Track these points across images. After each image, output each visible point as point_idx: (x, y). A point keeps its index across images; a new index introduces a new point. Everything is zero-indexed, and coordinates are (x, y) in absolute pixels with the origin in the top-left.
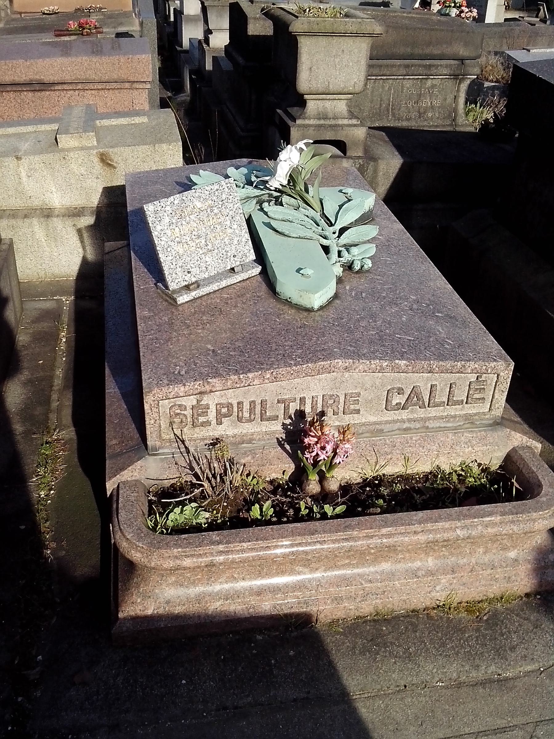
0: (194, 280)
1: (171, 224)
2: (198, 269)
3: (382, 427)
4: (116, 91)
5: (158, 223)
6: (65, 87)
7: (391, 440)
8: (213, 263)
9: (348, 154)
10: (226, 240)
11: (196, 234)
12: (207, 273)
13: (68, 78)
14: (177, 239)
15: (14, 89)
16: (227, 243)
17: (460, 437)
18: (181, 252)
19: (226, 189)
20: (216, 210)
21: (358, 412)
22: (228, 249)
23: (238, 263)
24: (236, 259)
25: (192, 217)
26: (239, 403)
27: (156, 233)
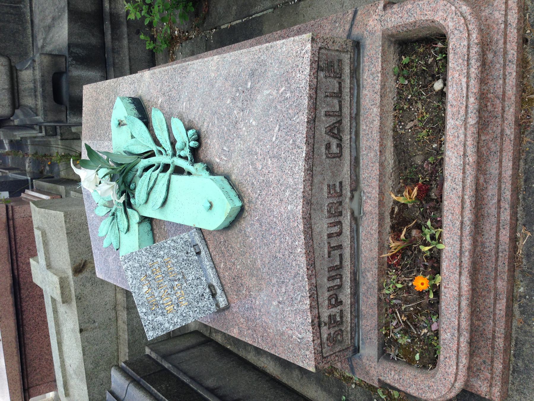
0: (208, 290)
1: (163, 314)
2: (199, 286)
3: (353, 158)
4: (16, 230)
5: (162, 327)
6: (15, 267)
7: (364, 149)
8: (193, 273)
9: (64, 70)
10: (174, 262)
11: (170, 290)
12: (202, 278)
13: (8, 267)
14: (175, 308)
15: (19, 303)
16: (176, 260)
17: (368, 83)
18: (185, 303)
19: (130, 263)
20: (149, 272)
21: (341, 183)
22: (181, 259)
23: (192, 249)
24: (189, 251)
26: (328, 291)
27: (171, 327)
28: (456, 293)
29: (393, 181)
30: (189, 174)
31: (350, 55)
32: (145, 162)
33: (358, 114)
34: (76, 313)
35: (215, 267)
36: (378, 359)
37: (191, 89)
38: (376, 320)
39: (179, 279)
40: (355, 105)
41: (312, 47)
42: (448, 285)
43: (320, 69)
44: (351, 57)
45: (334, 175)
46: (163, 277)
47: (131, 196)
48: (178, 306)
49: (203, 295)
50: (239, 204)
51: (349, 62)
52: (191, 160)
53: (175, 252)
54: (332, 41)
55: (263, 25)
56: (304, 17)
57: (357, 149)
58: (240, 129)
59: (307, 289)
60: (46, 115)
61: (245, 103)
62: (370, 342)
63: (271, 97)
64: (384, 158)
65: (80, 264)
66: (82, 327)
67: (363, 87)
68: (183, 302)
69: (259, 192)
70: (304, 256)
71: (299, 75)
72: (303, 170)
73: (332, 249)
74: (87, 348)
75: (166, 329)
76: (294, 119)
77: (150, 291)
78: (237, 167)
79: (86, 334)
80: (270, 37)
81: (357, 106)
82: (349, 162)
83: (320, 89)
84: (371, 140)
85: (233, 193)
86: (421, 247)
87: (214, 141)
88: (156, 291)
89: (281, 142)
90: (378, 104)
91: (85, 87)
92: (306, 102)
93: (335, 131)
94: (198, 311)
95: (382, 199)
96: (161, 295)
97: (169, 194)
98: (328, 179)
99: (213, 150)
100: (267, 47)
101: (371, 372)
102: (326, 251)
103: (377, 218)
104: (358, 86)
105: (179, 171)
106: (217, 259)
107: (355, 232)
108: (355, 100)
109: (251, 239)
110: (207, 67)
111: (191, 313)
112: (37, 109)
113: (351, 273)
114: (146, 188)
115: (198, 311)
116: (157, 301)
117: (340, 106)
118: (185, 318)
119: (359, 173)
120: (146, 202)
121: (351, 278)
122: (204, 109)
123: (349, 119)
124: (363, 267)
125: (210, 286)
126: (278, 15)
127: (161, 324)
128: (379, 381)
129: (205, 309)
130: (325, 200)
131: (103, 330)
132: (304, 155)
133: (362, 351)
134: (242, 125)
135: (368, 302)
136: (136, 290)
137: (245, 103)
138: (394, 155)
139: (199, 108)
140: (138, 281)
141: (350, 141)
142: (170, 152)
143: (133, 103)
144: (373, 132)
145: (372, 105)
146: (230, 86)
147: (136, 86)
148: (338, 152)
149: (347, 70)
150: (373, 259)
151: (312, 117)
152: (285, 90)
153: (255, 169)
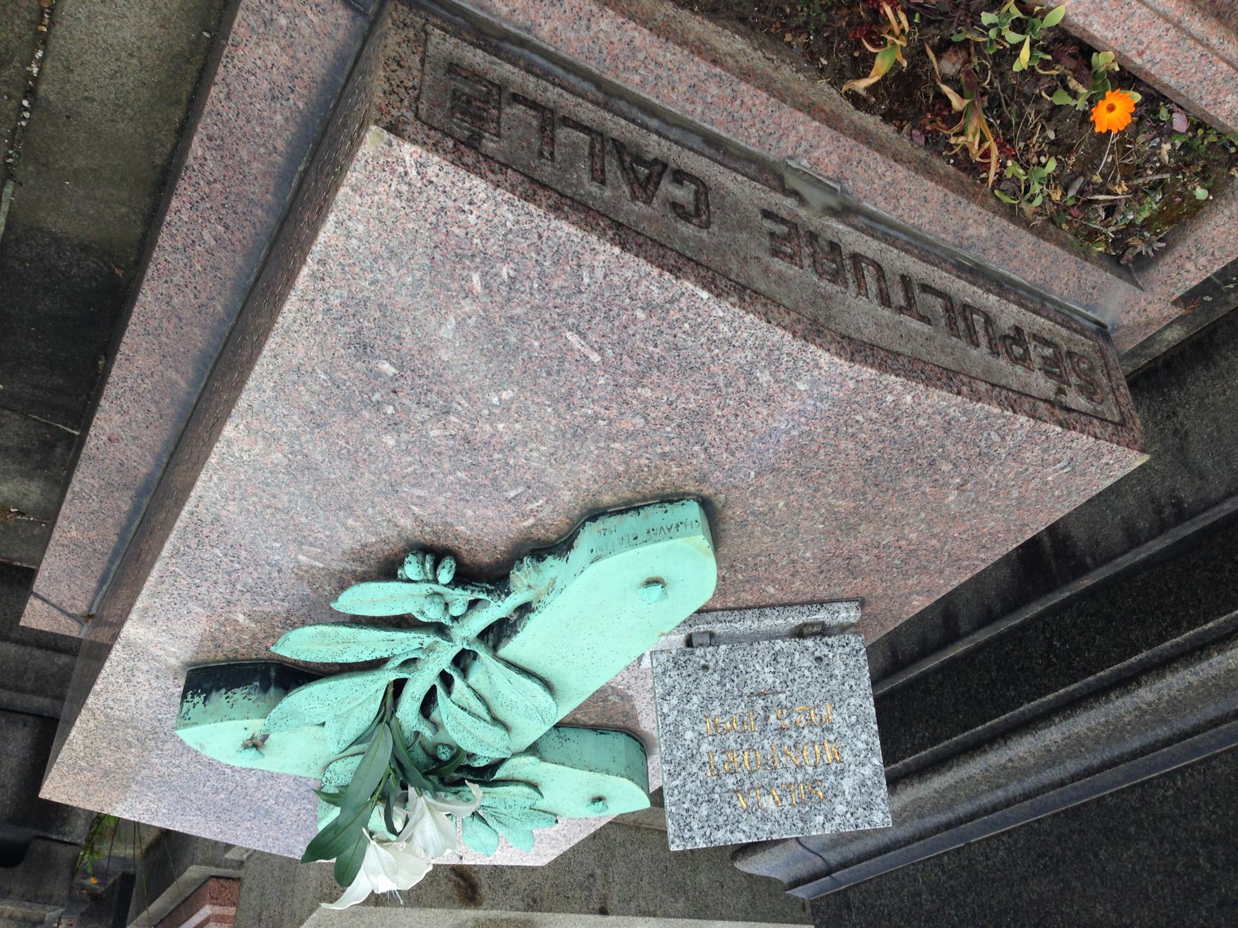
0: (809, 643)
1: (840, 774)
2: (795, 661)
3: (707, 151)
5: (869, 783)
7: (689, 107)
8: (758, 667)
10: (719, 710)
11: (786, 740)
12: (777, 648)
14: (832, 738)
16: (716, 703)
18: (826, 710)
20: (730, 781)
21: (767, 214)
22: (718, 688)
23: (699, 652)
24: (703, 662)
25: (789, 778)
28: (1173, 32)
29: (783, 61)
30: (525, 609)
31: (435, 26)
32: (408, 709)
33: (598, 82)
34: (561, 916)
35: (760, 608)
36: (1136, 285)
37: (272, 530)
38: (1067, 255)
39: (765, 709)
40: (572, 79)
41: (414, 142)
42: (1141, 43)
43: (473, 142)
44: (442, 29)
45: (743, 226)
46: (751, 749)
47: (466, 762)
48: (829, 730)
49: (819, 659)
50: (692, 511)
51: (453, 40)
52: (489, 592)
53: (695, 699)
54: (394, 67)
55: (41, 230)
56: (91, 100)
57: (687, 127)
58: (493, 436)
59: (997, 410)
60: (51, 897)
61: (433, 397)
62: (1100, 290)
63: (471, 322)
64: (730, 61)
65: (458, 886)
66: (597, 907)
67: (529, 30)
68: (824, 713)
69: (696, 448)
70: (931, 389)
71: (472, 219)
72: (742, 313)
73: (909, 307)
74: (643, 904)
75: (876, 774)
76: (586, 280)
77: (776, 793)
78: (574, 481)
79: (613, 902)
80: (172, 236)
81: (575, 74)
82: (716, 168)
83: (529, 167)
84: (676, 77)
85: (655, 516)
86: (1017, 67)
87: (470, 513)
88: (782, 776)
89: (621, 342)
90: (594, 8)
91: (40, 796)
92: (565, 229)
93: (646, 174)
94: (853, 683)
95: (823, 115)
96: (793, 767)
97: (538, 672)
98: (757, 247)
99: (483, 525)
100: (313, 275)
101: (1151, 316)
102: (916, 324)
103: (865, 149)
104: (522, 43)
105: (496, 634)
106: (748, 598)
107: (873, 225)
108: (560, 71)
109: (781, 504)
110: (242, 463)
111: (852, 701)
112: (24, 920)
113: (958, 277)
114: (483, 723)
115: (853, 683)
116: (804, 782)
117: (578, 126)
118: (861, 719)
119: (739, 148)
120: (506, 727)
121: (970, 282)
122: (359, 512)
123: (608, 116)
124: (949, 238)
125: (799, 633)
126: (39, 173)
127: (863, 784)
128: (1175, 303)
129: (852, 663)
130: (799, 276)
131: (613, 857)
132: (705, 295)
133: (1106, 320)
134: (487, 427)
135: (1023, 260)
136: (767, 828)
137: (433, 397)
138: (724, 27)
139: (344, 525)
140: (745, 816)
141: (667, 138)
142: (428, 639)
143: (208, 692)
144: (660, 59)
145: (588, 28)
146: (347, 421)
147: (145, 668)
148: (693, 186)
149: (476, 58)
150: (945, 203)
151: (611, 228)
152: (484, 275)
153: (631, 435)
